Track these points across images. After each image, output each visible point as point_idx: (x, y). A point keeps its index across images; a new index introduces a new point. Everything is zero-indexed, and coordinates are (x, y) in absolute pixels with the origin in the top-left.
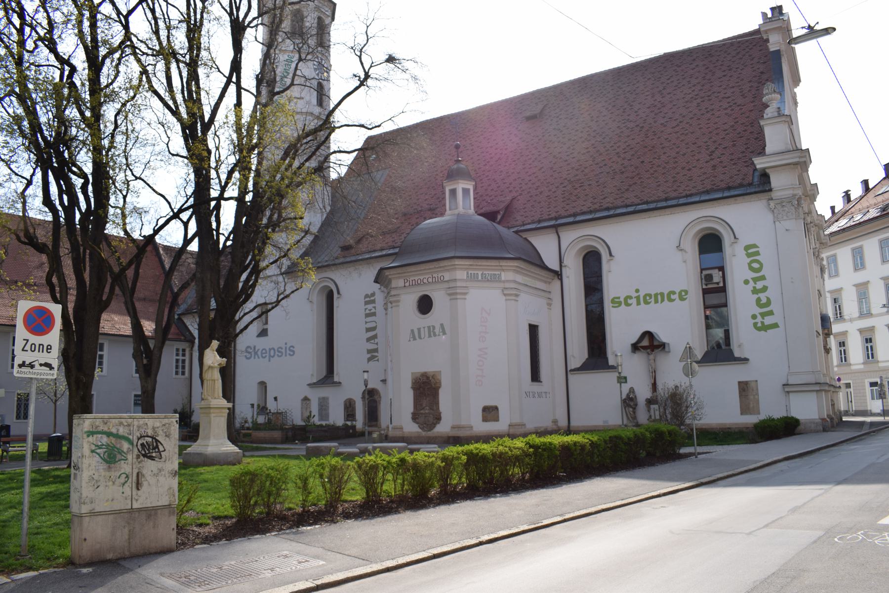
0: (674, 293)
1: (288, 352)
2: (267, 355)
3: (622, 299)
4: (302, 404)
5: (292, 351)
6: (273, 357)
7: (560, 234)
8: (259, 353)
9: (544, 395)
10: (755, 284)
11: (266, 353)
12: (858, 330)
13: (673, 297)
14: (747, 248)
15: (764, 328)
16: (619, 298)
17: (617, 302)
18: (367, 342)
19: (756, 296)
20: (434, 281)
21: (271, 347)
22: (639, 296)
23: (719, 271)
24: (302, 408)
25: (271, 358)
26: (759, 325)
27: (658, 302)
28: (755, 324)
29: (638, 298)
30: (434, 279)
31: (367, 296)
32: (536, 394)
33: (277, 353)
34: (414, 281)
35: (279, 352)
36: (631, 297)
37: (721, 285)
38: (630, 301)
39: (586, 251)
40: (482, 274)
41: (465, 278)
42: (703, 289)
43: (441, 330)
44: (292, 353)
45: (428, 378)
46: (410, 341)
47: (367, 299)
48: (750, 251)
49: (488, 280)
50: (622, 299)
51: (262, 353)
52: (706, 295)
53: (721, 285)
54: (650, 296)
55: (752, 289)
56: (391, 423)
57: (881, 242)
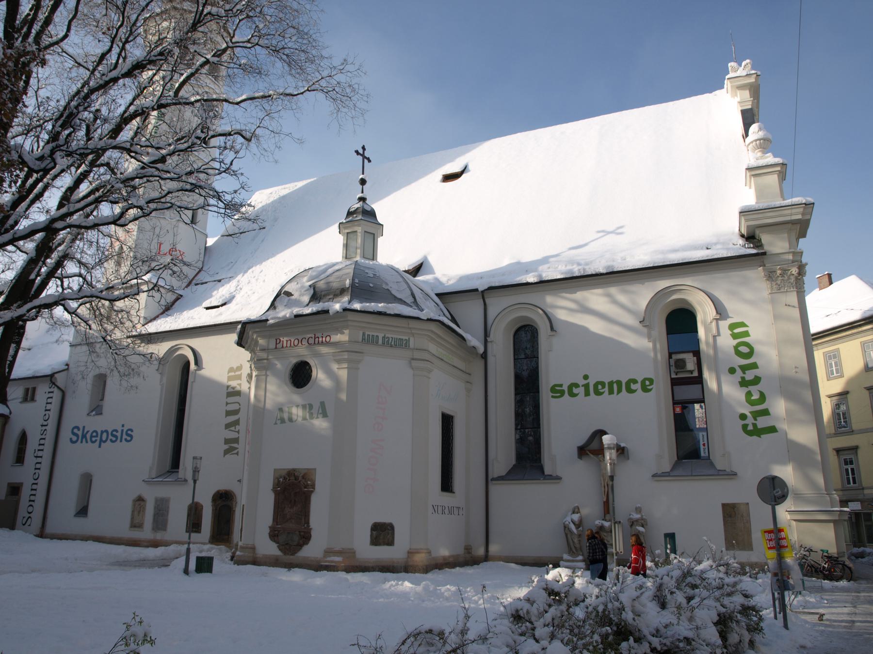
0: (635, 381)
1: (125, 436)
2: (98, 439)
3: (565, 388)
4: (134, 505)
5: (129, 435)
6: (105, 442)
7: (487, 301)
8: (88, 436)
9: (456, 512)
10: (744, 373)
11: (97, 436)
12: (834, 449)
13: (633, 387)
14: (732, 327)
15: (757, 432)
16: (561, 386)
17: (559, 391)
18: (226, 429)
19: (745, 390)
20: (316, 342)
21: (104, 430)
22: (588, 384)
23: (694, 356)
24: (133, 511)
25: (102, 444)
26: (750, 428)
27: (747, 332)
28: (745, 427)
29: (586, 386)
30: (317, 339)
31: (231, 370)
32: (447, 508)
33: (110, 437)
34: (289, 342)
35: (113, 435)
36: (576, 385)
37: (696, 374)
38: (575, 391)
39: (523, 324)
40: (384, 338)
41: (360, 339)
42: (672, 379)
43: (320, 411)
44: (129, 438)
45: (296, 478)
46: (276, 424)
47: (231, 374)
48: (736, 331)
49: (391, 346)
50: (565, 388)
51: (92, 436)
52: (674, 387)
53: (696, 374)
54: (603, 384)
55: (740, 380)
56: (241, 540)
57: (863, 345)
